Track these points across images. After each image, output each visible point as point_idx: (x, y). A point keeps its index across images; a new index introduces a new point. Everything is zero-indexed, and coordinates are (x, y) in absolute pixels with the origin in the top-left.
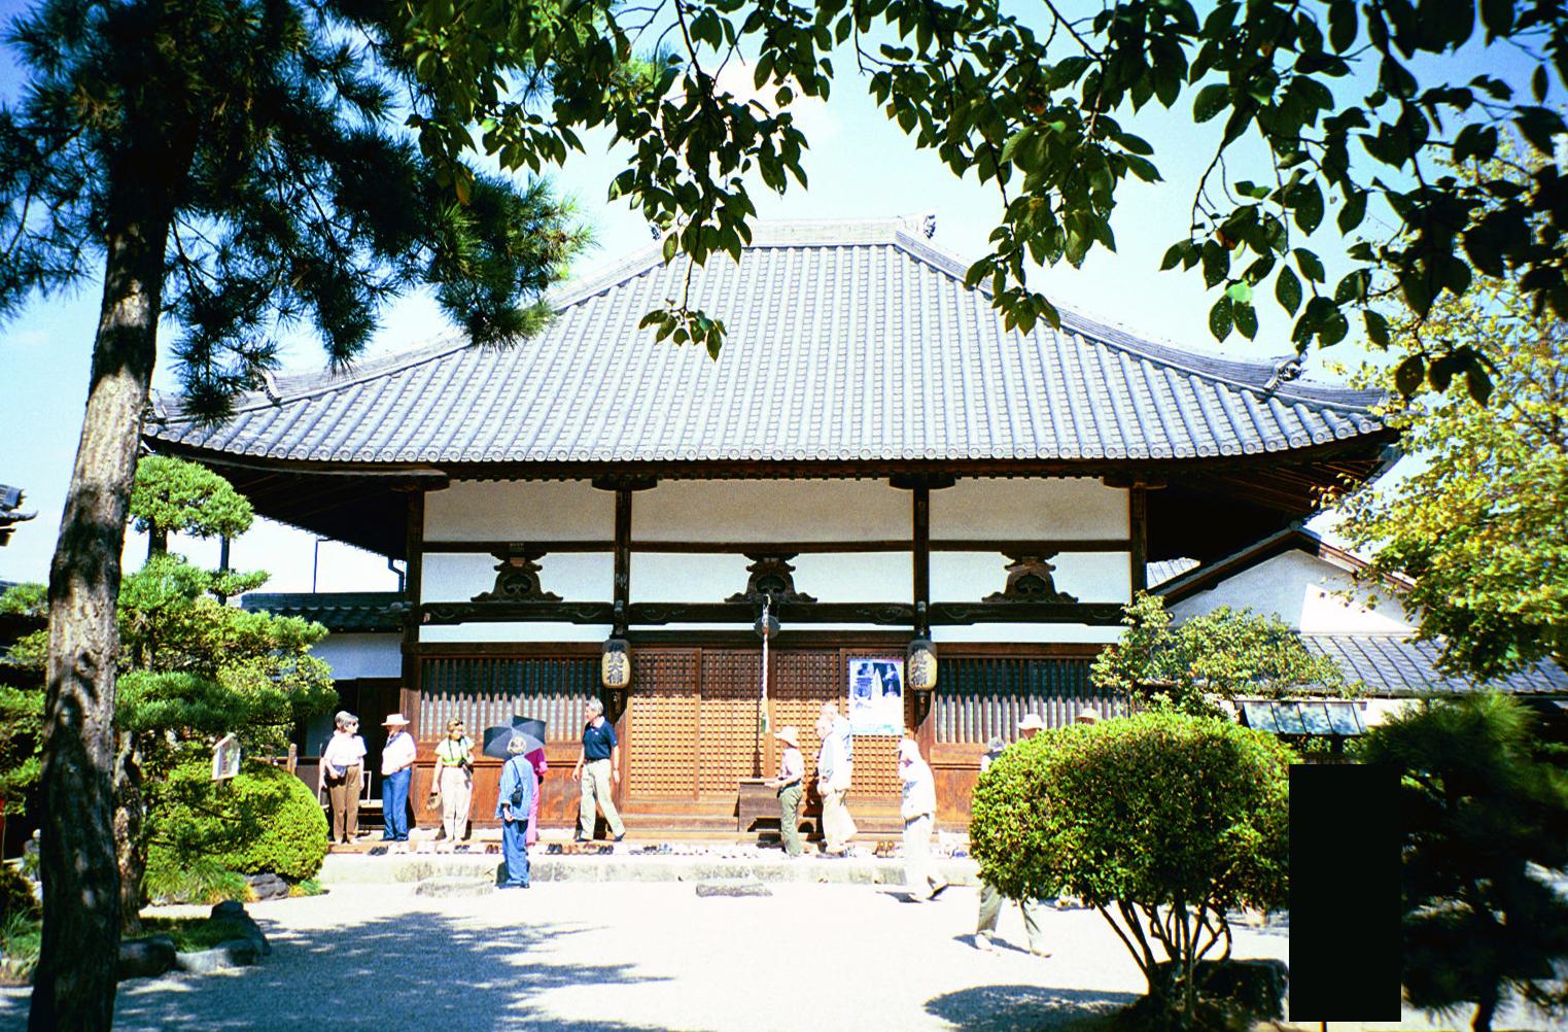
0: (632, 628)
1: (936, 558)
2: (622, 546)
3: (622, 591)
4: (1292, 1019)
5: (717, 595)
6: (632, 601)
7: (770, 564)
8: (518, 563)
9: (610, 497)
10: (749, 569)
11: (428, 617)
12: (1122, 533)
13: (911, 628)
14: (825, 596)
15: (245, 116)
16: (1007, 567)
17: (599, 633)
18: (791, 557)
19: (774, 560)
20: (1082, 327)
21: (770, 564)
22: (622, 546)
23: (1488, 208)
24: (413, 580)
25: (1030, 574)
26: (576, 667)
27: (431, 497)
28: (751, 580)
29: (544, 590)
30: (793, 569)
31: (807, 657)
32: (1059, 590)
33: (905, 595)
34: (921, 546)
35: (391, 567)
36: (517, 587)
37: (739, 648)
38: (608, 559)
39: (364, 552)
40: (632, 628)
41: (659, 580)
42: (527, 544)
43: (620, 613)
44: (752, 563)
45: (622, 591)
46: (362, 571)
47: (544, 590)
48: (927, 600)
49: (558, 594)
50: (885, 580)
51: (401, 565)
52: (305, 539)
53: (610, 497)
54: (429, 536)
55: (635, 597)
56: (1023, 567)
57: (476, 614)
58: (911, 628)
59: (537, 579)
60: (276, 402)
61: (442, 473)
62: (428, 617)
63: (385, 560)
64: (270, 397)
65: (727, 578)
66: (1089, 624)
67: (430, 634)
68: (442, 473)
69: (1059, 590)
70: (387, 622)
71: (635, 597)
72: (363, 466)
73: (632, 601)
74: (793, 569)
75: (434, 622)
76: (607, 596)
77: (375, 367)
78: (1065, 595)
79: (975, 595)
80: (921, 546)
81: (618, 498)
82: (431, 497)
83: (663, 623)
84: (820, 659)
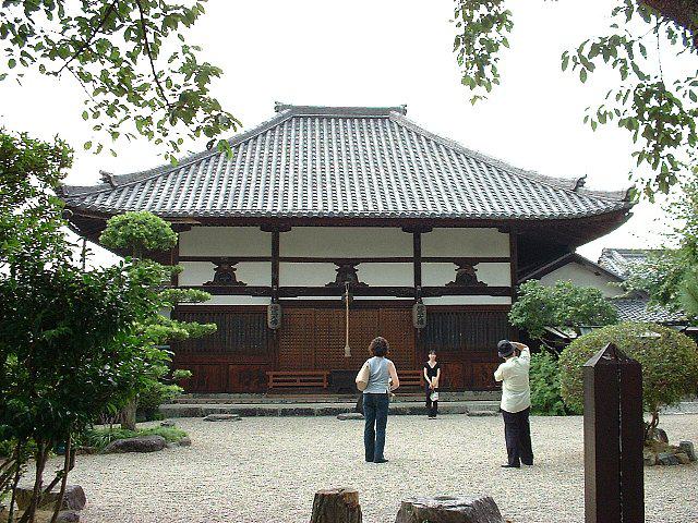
2: (275, 260)
3: (275, 281)
5: (321, 284)
7: (347, 267)
21: (347, 267)
22: (275, 260)
33: (269, 284)
34: (417, 260)
41: (292, 276)
43: (275, 291)
45: (275, 281)
50: (401, 276)
55: (425, 283)
65: (325, 275)
67: (429, 301)
71: (425, 283)
76: (269, 284)
80: (417, 260)
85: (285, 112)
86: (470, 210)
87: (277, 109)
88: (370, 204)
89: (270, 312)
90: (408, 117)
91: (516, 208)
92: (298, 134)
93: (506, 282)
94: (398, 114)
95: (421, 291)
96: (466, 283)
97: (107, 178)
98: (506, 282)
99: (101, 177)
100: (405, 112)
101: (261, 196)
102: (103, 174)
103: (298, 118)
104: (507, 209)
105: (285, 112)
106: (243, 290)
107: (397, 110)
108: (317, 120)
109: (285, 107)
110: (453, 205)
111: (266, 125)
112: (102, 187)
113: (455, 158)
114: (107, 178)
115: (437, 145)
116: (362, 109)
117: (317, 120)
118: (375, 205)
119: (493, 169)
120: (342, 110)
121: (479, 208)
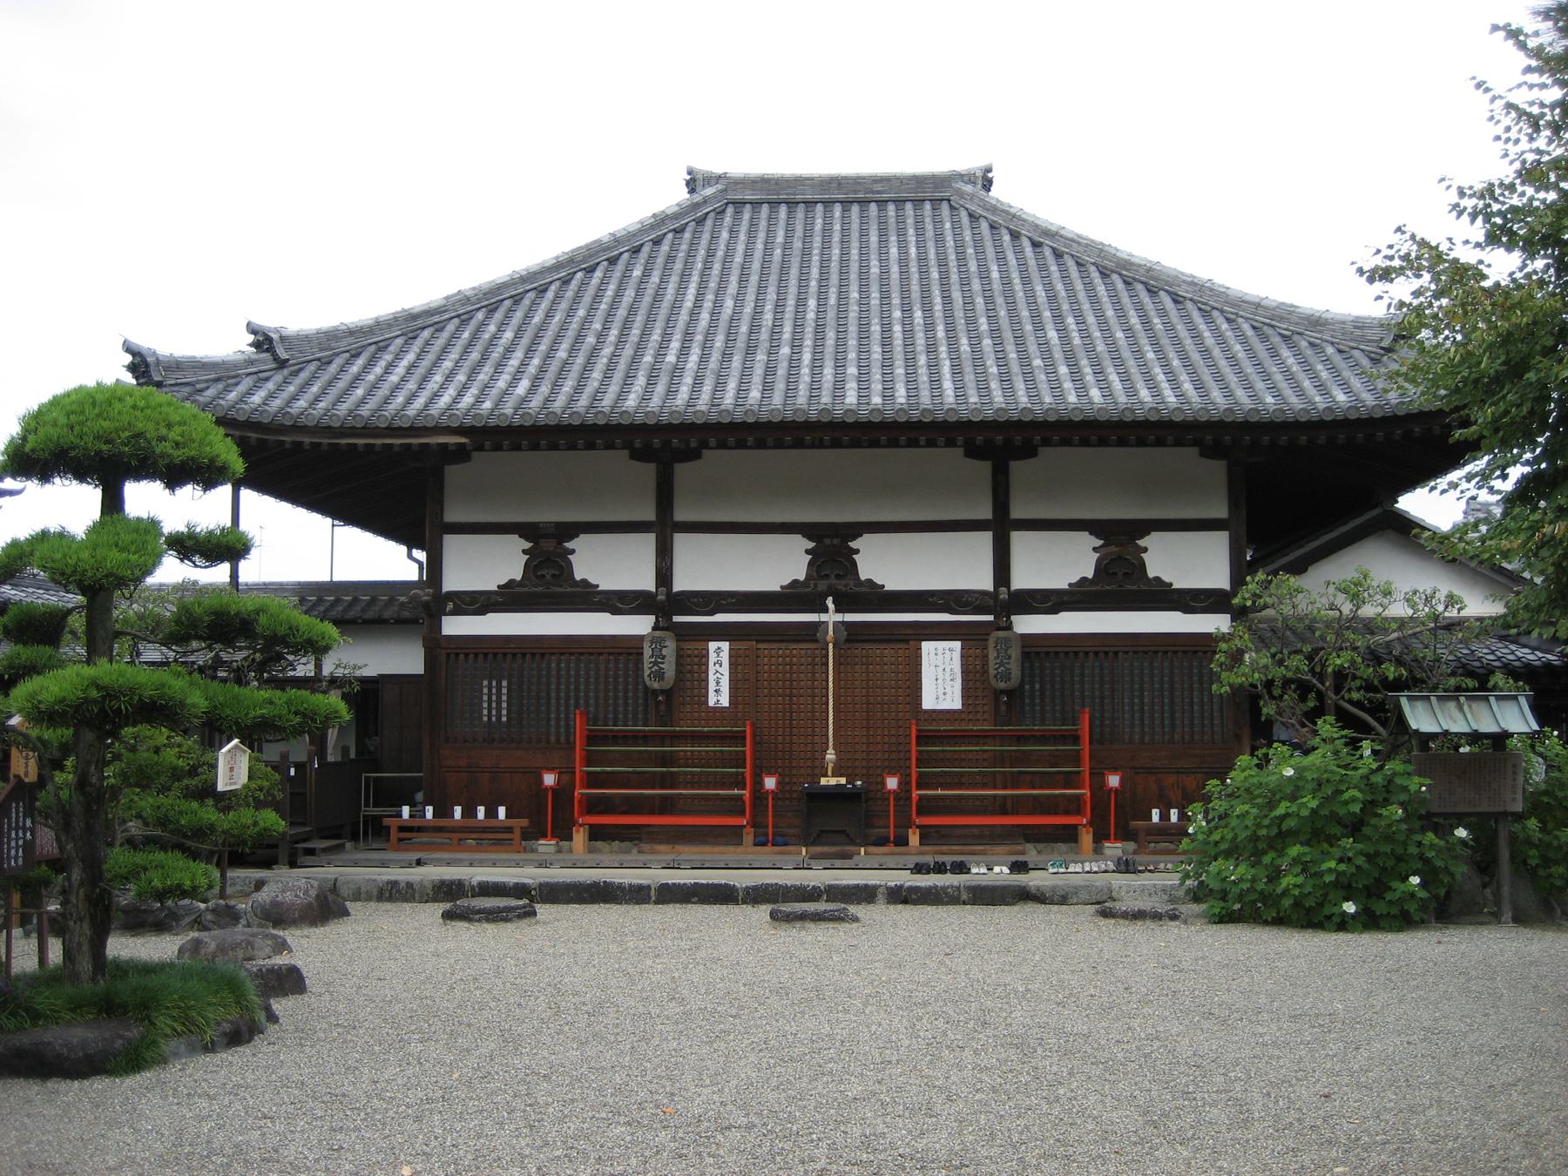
0: (677, 619)
1: (1019, 540)
2: (665, 529)
3: (664, 575)
4: (837, 611)
5: (772, 582)
6: (677, 588)
7: (832, 548)
8: (548, 545)
9: (648, 471)
10: (524, 552)
11: (450, 606)
12: (1221, 512)
13: (990, 618)
14: (893, 582)
15: (1553, 429)
16: (1095, 549)
17: (638, 625)
18: (854, 538)
19: (836, 541)
20: (1167, 283)
21: (832, 548)
22: (665, 529)
23: (1554, 155)
24: (434, 568)
25: (1120, 557)
26: (617, 662)
27: (454, 474)
28: (810, 564)
29: (578, 577)
30: (857, 552)
31: (875, 650)
32: (1151, 574)
33: (647, 583)
34: (1002, 528)
35: (410, 556)
36: (547, 573)
37: (798, 641)
39: (381, 540)
40: (677, 619)
41: (706, 566)
42: (558, 525)
43: (663, 602)
44: (811, 545)
45: (664, 575)
46: (380, 559)
47: (578, 577)
48: (1008, 586)
49: (1166, 579)
51: (421, 555)
52: (319, 523)
53: (648, 471)
54: (451, 516)
55: (681, 584)
56: (1113, 549)
57: (501, 604)
58: (990, 618)
59: (570, 564)
60: (282, 364)
61: (463, 440)
62: (450, 606)
63: (404, 549)
64: (276, 358)
65: (778, 564)
66: (1185, 612)
67: (1029, 624)
68: (463, 440)
69: (1151, 574)
70: (406, 614)
71: (681, 584)
72: (367, 430)
73: (677, 588)
74: (857, 552)
75: (458, 612)
76: (647, 583)
77: (390, 326)
78: (1158, 579)
79: (488, 581)
80: (1002, 528)
81: (658, 472)
82: (453, 473)
83: (712, 613)
84: (888, 652)
85: (709, 191)
86: (1171, 399)
87: (692, 184)
88: (1044, 387)
89: (647, 652)
90: (995, 192)
91: (1288, 393)
92: (735, 240)
93: (1219, 578)
94: (968, 188)
95: (1008, 601)
96: (1119, 582)
97: (263, 341)
98: (1219, 578)
99: (251, 338)
100: (988, 184)
101: (618, 376)
102: (254, 332)
103: (739, 204)
104: (1241, 395)
105: (709, 191)
106: (1164, 597)
107: (968, 178)
108: (928, 206)
109: (710, 179)
110: (1153, 386)
111: (660, 220)
112: (250, 362)
113: (1097, 279)
114: (263, 341)
115: (1058, 255)
116: (799, 182)
117: (928, 206)
118: (959, 388)
119: (1189, 305)
120: (838, 182)
121: (1144, 394)
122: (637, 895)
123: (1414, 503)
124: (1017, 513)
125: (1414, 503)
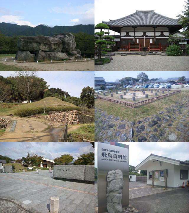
2: (135, 32)
7: (145, 33)
12: (168, 31)
21: (145, 33)
33: (133, 35)
34: (155, 32)
38: (134, 33)
43: (134, 36)
65: (142, 34)
67: (122, 38)
80: (155, 32)
122: (133, 54)
123: (180, 30)
124: (156, 31)
125: (180, 30)
